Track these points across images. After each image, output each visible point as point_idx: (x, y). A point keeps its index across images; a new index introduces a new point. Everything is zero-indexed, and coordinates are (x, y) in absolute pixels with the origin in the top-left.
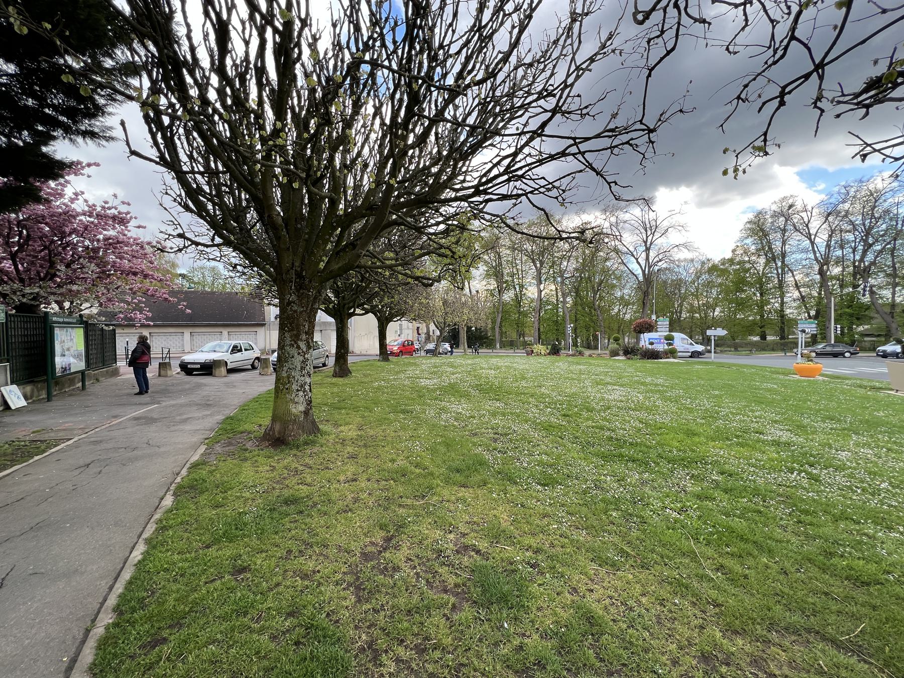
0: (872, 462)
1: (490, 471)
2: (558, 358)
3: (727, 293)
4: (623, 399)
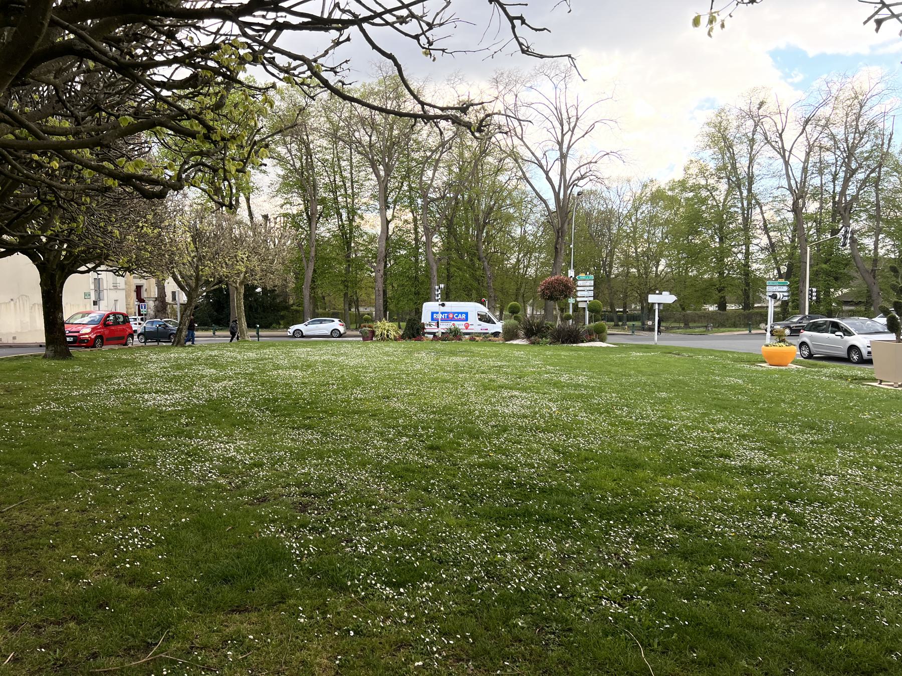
0: (862, 488)
1: (293, 571)
2: (418, 344)
3: (676, 237)
4: (528, 412)
